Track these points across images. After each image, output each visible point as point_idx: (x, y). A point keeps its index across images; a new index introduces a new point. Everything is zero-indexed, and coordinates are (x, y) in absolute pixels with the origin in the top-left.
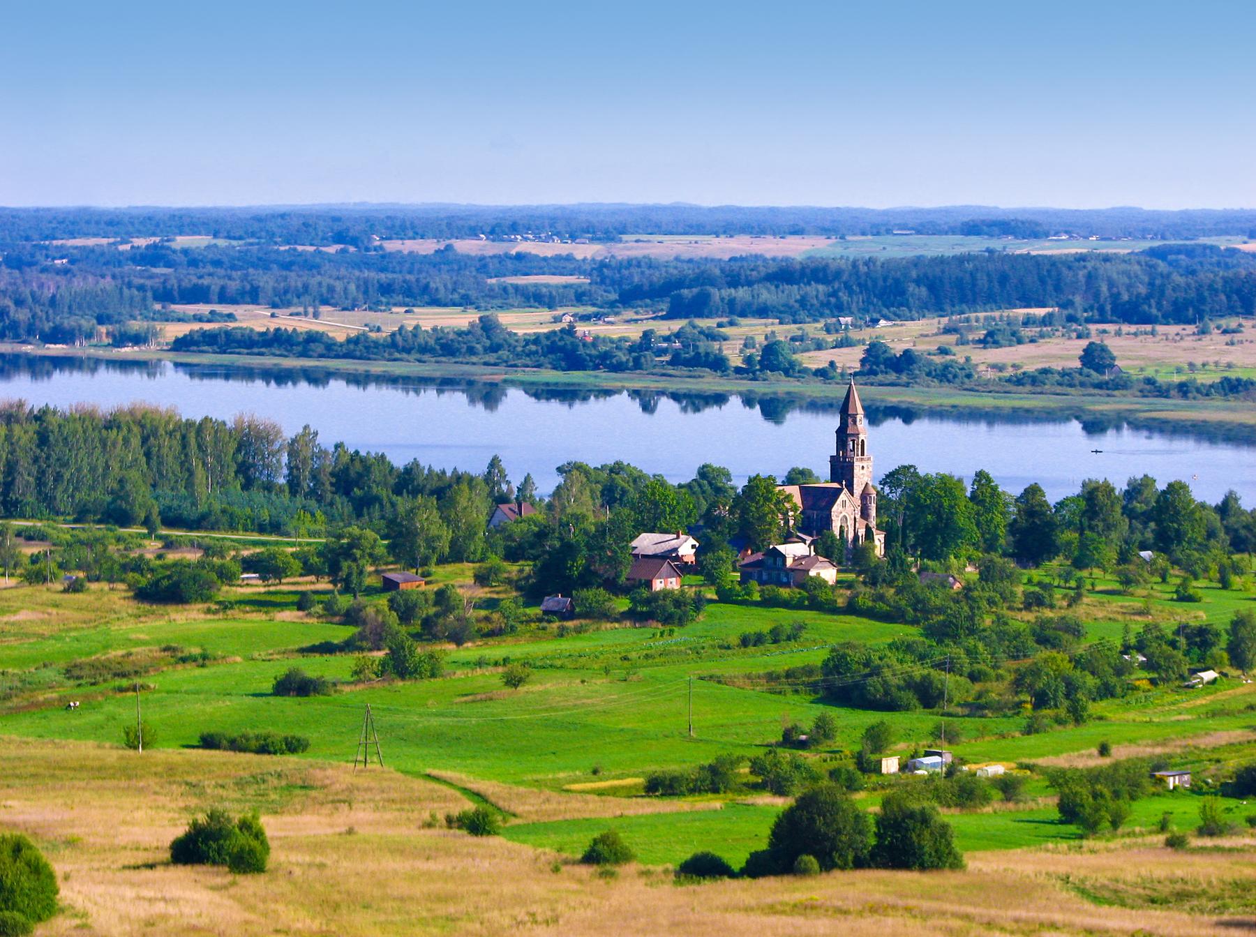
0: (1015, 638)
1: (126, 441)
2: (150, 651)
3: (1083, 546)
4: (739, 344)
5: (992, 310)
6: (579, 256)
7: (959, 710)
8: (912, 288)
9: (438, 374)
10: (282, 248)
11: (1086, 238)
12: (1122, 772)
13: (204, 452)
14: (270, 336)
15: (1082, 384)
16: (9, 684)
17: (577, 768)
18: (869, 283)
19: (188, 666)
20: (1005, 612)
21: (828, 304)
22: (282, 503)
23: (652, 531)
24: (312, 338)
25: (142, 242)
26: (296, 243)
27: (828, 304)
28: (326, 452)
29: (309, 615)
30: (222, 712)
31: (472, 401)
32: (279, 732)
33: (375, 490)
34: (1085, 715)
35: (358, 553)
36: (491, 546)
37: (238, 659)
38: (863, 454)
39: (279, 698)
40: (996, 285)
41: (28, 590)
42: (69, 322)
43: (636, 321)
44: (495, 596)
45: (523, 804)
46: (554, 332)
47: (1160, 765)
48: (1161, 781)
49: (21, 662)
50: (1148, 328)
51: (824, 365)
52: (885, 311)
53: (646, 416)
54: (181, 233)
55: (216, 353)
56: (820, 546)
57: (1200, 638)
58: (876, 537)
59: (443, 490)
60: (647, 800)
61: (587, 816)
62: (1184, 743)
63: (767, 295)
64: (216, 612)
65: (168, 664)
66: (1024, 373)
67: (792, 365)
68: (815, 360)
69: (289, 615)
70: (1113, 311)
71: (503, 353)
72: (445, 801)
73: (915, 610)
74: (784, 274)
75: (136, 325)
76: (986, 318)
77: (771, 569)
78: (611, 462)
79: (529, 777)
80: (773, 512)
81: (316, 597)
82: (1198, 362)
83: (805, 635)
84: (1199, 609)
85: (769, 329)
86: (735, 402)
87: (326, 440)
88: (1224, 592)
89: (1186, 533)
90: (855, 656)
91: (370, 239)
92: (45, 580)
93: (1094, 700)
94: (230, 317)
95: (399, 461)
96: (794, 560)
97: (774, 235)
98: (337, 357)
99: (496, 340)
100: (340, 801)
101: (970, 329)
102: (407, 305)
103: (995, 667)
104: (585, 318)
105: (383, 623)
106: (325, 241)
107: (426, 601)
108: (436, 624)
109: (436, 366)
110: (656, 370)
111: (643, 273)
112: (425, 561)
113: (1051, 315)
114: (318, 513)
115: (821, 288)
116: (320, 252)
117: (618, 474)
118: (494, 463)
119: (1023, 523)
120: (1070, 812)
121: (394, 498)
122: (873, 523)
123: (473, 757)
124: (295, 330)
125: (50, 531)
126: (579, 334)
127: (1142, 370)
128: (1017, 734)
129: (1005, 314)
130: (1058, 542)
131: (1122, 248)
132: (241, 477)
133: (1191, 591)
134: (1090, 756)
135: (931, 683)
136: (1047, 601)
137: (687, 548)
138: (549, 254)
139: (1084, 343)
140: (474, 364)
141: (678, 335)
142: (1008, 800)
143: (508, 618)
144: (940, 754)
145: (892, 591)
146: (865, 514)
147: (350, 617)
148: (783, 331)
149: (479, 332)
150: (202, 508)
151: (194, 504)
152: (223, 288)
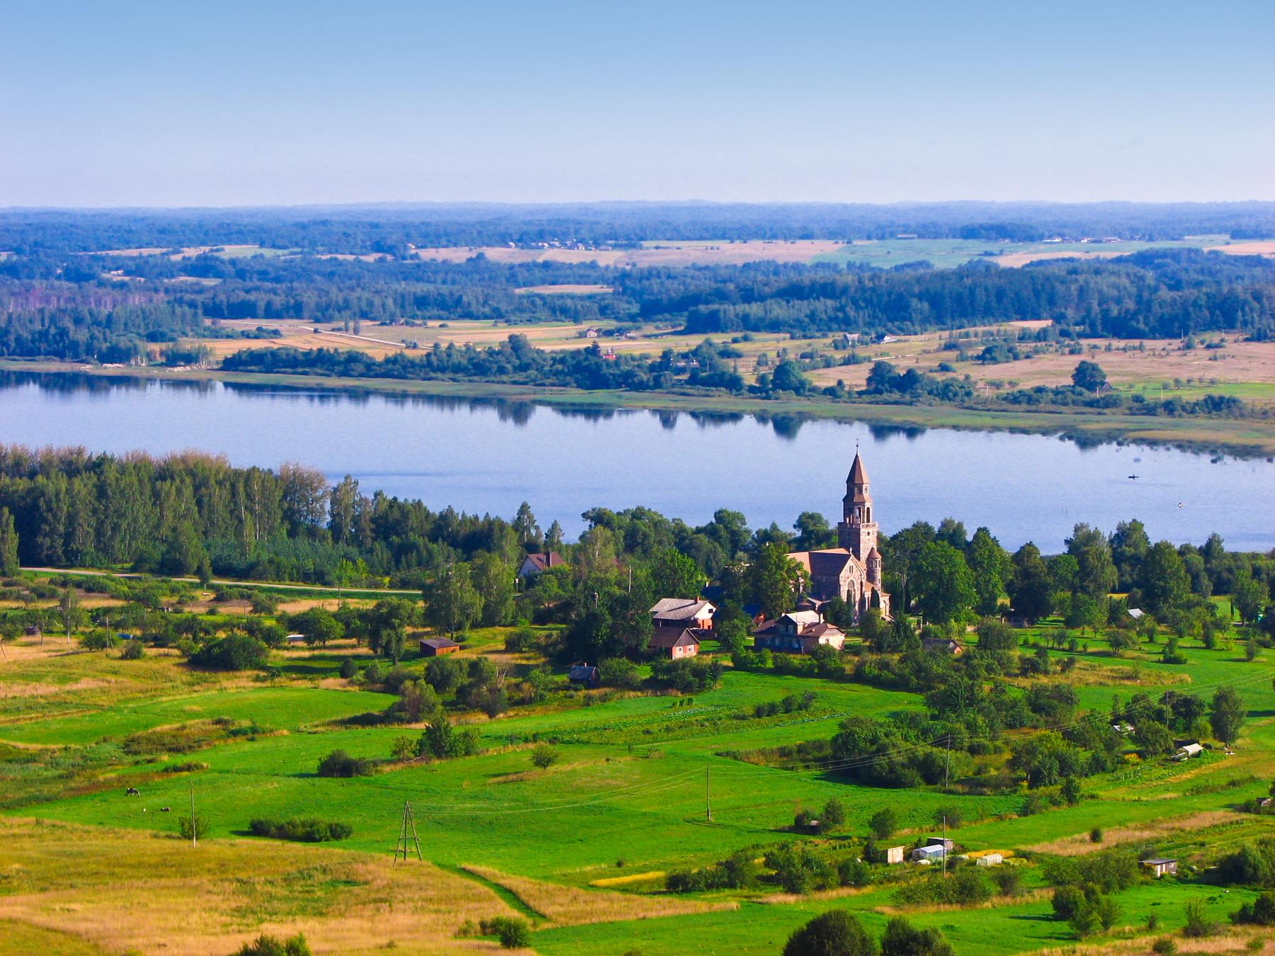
1: (179, 491)
2: (204, 724)
4: (752, 361)
6: (602, 263)
7: (960, 788)
8: (915, 302)
9: (471, 394)
10: (324, 258)
11: (1078, 240)
12: (1112, 863)
13: (252, 500)
14: (314, 355)
15: (1074, 403)
16: (71, 761)
17: (602, 860)
19: (239, 739)
20: (1002, 677)
21: (835, 319)
22: (325, 550)
23: (671, 596)
24: (353, 358)
25: (192, 252)
26: (337, 252)
27: (835, 319)
28: (366, 500)
29: (351, 683)
30: (270, 794)
31: (503, 417)
32: (324, 818)
33: (413, 537)
34: (1078, 795)
35: (397, 622)
36: (521, 609)
37: (286, 732)
39: (324, 780)
40: (993, 299)
41: (88, 656)
42: (123, 343)
43: (656, 336)
44: (524, 662)
45: (553, 903)
46: (578, 352)
47: (1146, 853)
48: (1148, 870)
49: (83, 736)
50: (1136, 342)
51: (832, 383)
53: (667, 431)
54: (229, 242)
55: (260, 373)
57: (1186, 708)
58: (881, 599)
59: (476, 539)
60: (667, 898)
61: (611, 919)
62: (1170, 825)
63: (778, 310)
64: (264, 680)
65: (221, 738)
68: (824, 378)
69: (333, 682)
70: (1104, 328)
71: (532, 373)
72: (479, 901)
73: (917, 678)
74: (794, 292)
75: (188, 344)
76: (985, 334)
77: (783, 637)
78: (633, 507)
79: (557, 872)
80: (784, 580)
81: (357, 663)
82: (1184, 379)
83: (815, 704)
84: (1184, 671)
85: (782, 345)
86: (748, 422)
87: (366, 490)
88: (1208, 653)
89: (1171, 590)
90: (862, 733)
91: (406, 247)
92: (104, 646)
93: (1086, 775)
94: (276, 333)
95: (435, 507)
97: (786, 239)
98: (377, 376)
100: (381, 900)
101: (970, 345)
102: (440, 318)
103: (994, 739)
104: (609, 333)
105: (421, 696)
106: (365, 250)
107: (461, 669)
108: (470, 694)
109: (468, 386)
110: (675, 390)
112: (460, 627)
113: (1044, 331)
114: (360, 561)
115: (830, 303)
116: (360, 261)
117: (639, 519)
118: (524, 509)
119: (1018, 583)
120: (1063, 909)
121: (430, 545)
123: (505, 845)
125: (109, 582)
127: (1131, 386)
128: (1015, 817)
129: (1002, 328)
131: (1109, 252)
132: (286, 523)
133: (1178, 652)
134: (1082, 841)
135: (933, 761)
136: (1042, 667)
137: (704, 613)
138: (575, 261)
139: (1075, 361)
140: (504, 383)
141: (695, 353)
142: (1006, 893)
143: (537, 687)
144: (941, 843)
145: (896, 657)
146: (871, 577)
147: (391, 685)
150: (251, 558)
151: (243, 554)
152: (269, 304)
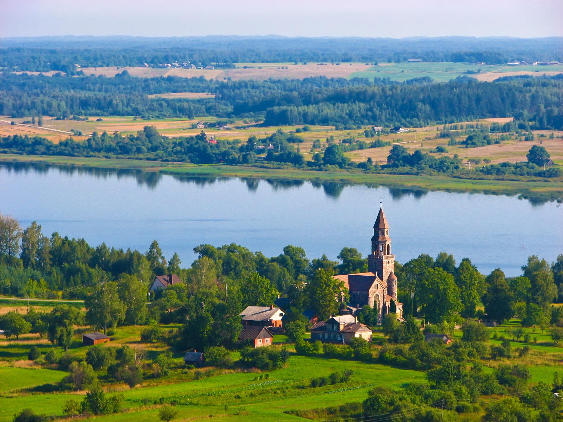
0: (486, 381)
3: (529, 312)
4: (310, 145)
5: (472, 121)
6: (208, 77)
8: (420, 105)
9: (118, 167)
10: (18, 73)
15: (528, 174)
18: (393, 102)
24: (37, 142)
26: (27, 70)
28: (46, 239)
31: (140, 182)
33: (78, 264)
38: (388, 254)
43: (244, 128)
44: (154, 349)
46: (192, 138)
51: (364, 160)
52: (403, 121)
56: (361, 317)
58: (397, 307)
59: (121, 266)
63: (328, 110)
66: (492, 166)
67: (344, 160)
70: (549, 122)
71: (160, 152)
73: (422, 361)
78: (228, 244)
81: (40, 350)
85: (330, 134)
87: (46, 232)
90: (384, 398)
91: (74, 67)
95: (94, 243)
96: (345, 327)
97: (332, 62)
98: (54, 154)
99: (155, 144)
101: (458, 134)
102: (97, 115)
103: (473, 402)
104: (212, 126)
105: (84, 372)
106: (47, 68)
107: (111, 354)
108: (117, 371)
111: (248, 91)
112: (110, 325)
114: (42, 280)
115: (362, 105)
116: (43, 76)
117: (232, 252)
118: (154, 245)
119: (490, 296)
121: (91, 270)
122: (395, 298)
124: (26, 136)
126: (208, 138)
130: (513, 309)
135: (432, 417)
136: (506, 353)
137: (277, 316)
139: (530, 144)
140: (141, 159)
141: (271, 139)
145: (407, 346)
146: (390, 292)
147: (63, 365)
148: (337, 135)
149: (144, 138)
